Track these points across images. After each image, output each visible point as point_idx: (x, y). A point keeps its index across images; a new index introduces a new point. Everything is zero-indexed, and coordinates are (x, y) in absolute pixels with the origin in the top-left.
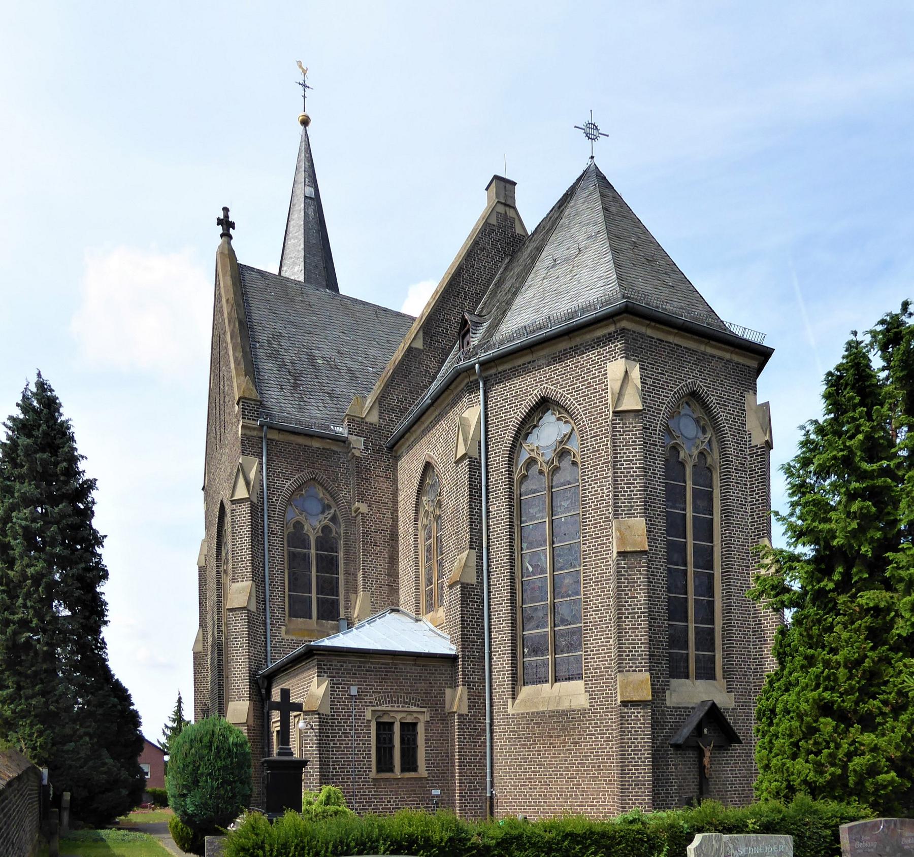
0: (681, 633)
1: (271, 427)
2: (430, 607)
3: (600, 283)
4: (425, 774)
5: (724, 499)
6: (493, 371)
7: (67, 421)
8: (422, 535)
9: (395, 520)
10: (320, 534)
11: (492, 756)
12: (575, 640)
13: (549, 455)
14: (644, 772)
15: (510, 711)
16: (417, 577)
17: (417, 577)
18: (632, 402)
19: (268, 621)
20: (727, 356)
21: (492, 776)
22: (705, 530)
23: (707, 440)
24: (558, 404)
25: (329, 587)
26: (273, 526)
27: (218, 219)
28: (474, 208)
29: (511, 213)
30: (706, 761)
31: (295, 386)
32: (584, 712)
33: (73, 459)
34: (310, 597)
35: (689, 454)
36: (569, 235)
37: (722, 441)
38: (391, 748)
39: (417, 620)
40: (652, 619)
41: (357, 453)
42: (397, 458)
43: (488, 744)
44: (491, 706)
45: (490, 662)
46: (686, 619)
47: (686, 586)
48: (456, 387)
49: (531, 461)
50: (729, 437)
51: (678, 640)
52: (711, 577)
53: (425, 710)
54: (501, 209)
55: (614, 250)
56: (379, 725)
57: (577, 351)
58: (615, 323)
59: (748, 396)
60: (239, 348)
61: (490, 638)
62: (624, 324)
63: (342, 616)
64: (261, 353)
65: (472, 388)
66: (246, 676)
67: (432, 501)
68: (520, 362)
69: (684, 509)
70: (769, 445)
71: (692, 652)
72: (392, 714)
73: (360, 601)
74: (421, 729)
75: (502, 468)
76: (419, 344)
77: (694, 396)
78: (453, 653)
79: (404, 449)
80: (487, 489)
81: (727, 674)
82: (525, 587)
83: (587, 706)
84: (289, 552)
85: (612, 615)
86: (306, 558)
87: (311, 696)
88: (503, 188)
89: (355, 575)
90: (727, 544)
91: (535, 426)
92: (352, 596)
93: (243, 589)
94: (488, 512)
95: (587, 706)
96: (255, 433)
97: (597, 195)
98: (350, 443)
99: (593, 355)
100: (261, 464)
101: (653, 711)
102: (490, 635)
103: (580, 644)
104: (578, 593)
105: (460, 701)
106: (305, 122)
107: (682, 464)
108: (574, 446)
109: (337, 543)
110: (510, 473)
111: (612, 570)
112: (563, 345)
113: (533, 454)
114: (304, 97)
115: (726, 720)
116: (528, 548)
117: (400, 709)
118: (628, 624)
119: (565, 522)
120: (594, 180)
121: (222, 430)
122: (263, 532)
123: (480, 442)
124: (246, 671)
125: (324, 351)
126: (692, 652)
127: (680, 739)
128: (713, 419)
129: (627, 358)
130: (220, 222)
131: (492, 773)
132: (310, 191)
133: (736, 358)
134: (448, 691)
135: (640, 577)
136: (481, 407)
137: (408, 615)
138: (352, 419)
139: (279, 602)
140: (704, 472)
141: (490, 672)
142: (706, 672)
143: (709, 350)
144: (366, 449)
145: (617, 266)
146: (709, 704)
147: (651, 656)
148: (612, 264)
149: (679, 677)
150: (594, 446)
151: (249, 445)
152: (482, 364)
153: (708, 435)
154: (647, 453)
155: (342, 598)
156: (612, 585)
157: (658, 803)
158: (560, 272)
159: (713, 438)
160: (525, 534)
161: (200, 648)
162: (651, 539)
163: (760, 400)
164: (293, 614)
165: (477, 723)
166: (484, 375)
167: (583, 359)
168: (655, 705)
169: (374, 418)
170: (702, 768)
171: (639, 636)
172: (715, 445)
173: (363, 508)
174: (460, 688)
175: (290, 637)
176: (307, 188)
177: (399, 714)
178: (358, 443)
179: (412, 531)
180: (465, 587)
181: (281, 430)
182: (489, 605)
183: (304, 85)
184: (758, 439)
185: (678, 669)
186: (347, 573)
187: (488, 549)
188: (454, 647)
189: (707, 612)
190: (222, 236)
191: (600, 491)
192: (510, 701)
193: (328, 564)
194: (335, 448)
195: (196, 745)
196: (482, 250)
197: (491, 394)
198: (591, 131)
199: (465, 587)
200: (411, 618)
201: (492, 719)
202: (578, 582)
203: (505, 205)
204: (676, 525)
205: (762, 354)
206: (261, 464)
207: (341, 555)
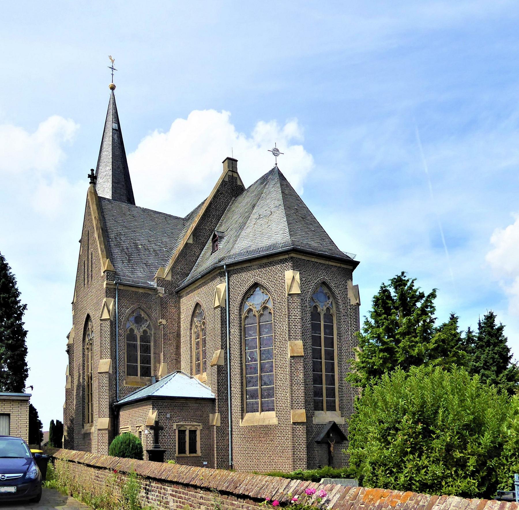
0: (319, 391)
1: (120, 284)
2: (198, 372)
3: (281, 232)
4: (200, 455)
5: (338, 329)
6: (232, 268)
7: (13, 275)
8: (194, 337)
9: (179, 327)
10: (142, 334)
11: (232, 446)
12: (270, 393)
13: (259, 308)
14: (303, 454)
15: (241, 425)
16: (191, 357)
17: (191, 357)
18: (296, 290)
19: (118, 378)
20: (339, 265)
21: (232, 456)
22: (330, 343)
23: (330, 303)
24: (262, 286)
25: (146, 360)
26: (120, 331)
27: (89, 175)
28: (217, 172)
29: (235, 175)
30: (332, 449)
31: (129, 260)
32: (276, 426)
33: (16, 294)
34: (137, 366)
35: (322, 309)
36: (266, 203)
37: (337, 303)
38: (185, 442)
39: (191, 378)
40: (306, 384)
41: (161, 295)
42: (180, 297)
43: (230, 440)
44: (231, 422)
45: (231, 402)
46: (322, 384)
47: (321, 368)
48: (213, 273)
49: (250, 310)
50: (340, 301)
51: (318, 393)
52: (333, 364)
53: (200, 424)
54: (230, 173)
55: (287, 216)
56: (180, 431)
57: (271, 264)
58: (288, 254)
59: (349, 282)
60: (103, 243)
61: (231, 391)
62: (293, 255)
63: (152, 375)
64: (112, 244)
65: (222, 275)
66: (108, 406)
67: (200, 321)
68: (245, 266)
69: (320, 334)
70: (359, 304)
71: (325, 398)
72: (185, 426)
73: (162, 368)
74: (198, 433)
75: (236, 312)
76: (191, 241)
77: (324, 283)
78: (213, 397)
79: (184, 293)
80: (229, 322)
81: (341, 409)
82: (247, 367)
83: (277, 423)
84: (127, 343)
85: (288, 383)
86: (135, 346)
87: (149, 418)
88: (231, 163)
89: (159, 355)
90: (340, 349)
91: (252, 295)
92: (158, 365)
93: (106, 363)
94: (230, 332)
95: (277, 423)
96: (112, 287)
97: (279, 185)
98: (158, 290)
99: (278, 267)
100: (115, 301)
101: (307, 426)
102: (231, 389)
103: (273, 395)
104: (272, 371)
105: (217, 420)
106: (113, 88)
107: (319, 314)
108: (270, 305)
109: (150, 338)
110: (240, 315)
111: (288, 363)
112: (265, 261)
113: (251, 307)
114: (113, 74)
115: (340, 430)
116: (248, 349)
117: (189, 424)
118: (295, 388)
119: (266, 339)
120: (276, 176)
121: (90, 279)
122: (116, 335)
123: (226, 300)
124: (108, 403)
125: (142, 241)
126: (325, 398)
127: (319, 439)
128: (333, 293)
129: (294, 270)
130: (89, 176)
131: (232, 454)
132: (115, 126)
133: (343, 266)
134: (211, 415)
135: (300, 367)
136: (227, 284)
137: (186, 375)
138: (159, 279)
139: (122, 369)
140: (329, 317)
141: (231, 406)
142: (331, 407)
143: (331, 263)
144: (165, 293)
145: (289, 224)
146: (333, 423)
147: (306, 401)
148: (286, 223)
149: (319, 410)
150: (278, 305)
151: (110, 292)
152: (226, 265)
153: (331, 300)
154: (303, 311)
155: (152, 365)
156: (288, 369)
157: (309, 467)
158: (263, 222)
159: (333, 302)
160: (247, 343)
161: (69, 387)
162: (305, 349)
163: (354, 283)
164: (129, 374)
165: (224, 430)
166: (228, 269)
167: (273, 268)
168: (308, 424)
169: (169, 278)
170: (330, 452)
171: (300, 393)
172: (334, 305)
173: (164, 322)
174: (217, 414)
175: (128, 386)
176: (114, 124)
177: (188, 426)
178: (161, 290)
179: (188, 333)
180: (219, 367)
181: (124, 285)
182: (230, 375)
183: (112, 68)
184: (353, 302)
185: (318, 407)
186: (155, 353)
187: (230, 349)
188: (214, 394)
189: (331, 380)
190: (90, 183)
191: (282, 326)
192: (240, 420)
193: (146, 349)
194: (150, 293)
195: (124, 444)
196: (221, 194)
197: (231, 278)
198: (276, 152)
199: (219, 367)
200: (188, 376)
201: (232, 428)
202: (272, 366)
203: (232, 171)
204: (316, 341)
205: (355, 264)
206: (115, 301)
207: (152, 344)
